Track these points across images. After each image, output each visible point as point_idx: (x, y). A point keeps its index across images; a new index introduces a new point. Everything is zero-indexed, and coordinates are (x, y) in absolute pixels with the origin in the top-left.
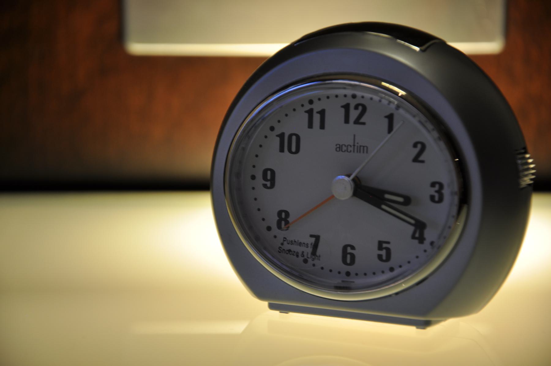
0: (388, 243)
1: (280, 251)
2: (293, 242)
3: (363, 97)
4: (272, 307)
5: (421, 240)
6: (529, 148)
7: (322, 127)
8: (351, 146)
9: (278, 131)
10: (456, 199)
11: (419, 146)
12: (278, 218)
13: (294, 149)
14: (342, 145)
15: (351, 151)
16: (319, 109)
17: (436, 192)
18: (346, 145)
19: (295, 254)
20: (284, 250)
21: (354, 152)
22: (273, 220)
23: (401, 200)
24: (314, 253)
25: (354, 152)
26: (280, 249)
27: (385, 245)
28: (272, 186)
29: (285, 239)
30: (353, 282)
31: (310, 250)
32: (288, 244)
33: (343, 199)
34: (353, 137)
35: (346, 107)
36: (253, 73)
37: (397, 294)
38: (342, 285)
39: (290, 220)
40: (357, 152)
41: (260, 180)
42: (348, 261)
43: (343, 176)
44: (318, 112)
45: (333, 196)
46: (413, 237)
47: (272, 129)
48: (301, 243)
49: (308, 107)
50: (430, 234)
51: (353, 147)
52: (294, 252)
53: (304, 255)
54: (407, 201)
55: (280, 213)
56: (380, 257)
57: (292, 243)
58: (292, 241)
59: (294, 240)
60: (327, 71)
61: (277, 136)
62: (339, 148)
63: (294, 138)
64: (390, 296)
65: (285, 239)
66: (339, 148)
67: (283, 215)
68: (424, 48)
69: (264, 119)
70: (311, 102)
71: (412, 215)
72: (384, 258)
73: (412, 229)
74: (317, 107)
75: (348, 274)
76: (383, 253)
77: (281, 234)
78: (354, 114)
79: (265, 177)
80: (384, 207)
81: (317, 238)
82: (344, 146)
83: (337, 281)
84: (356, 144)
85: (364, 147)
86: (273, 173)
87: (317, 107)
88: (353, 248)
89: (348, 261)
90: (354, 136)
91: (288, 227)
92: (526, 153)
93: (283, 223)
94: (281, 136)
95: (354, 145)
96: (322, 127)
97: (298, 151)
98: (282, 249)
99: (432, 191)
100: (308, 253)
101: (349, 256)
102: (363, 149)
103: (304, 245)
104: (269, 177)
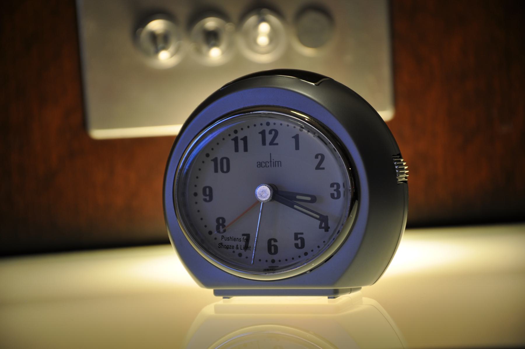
0: (302, 234)
1: (220, 247)
2: (229, 239)
3: (275, 124)
4: (217, 293)
6: (403, 155)
7: (246, 149)
8: (268, 162)
9: (212, 157)
10: (350, 196)
12: (217, 224)
13: (225, 169)
16: (242, 137)
17: (335, 190)
22: (213, 225)
23: (309, 199)
24: (246, 247)
28: (211, 199)
29: (223, 237)
32: (226, 240)
34: (270, 154)
35: (263, 133)
37: (311, 270)
39: (226, 224)
40: (274, 166)
41: (201, 196)
44: (241, 139)
46: (320, 227)
49: (234, 136)
51: (270, 163)
52: (231, 246)
53: (238, 248)
54: (314, 199)
55: (218, 220)
56: (296, 245)
57: (228, 239)
58: (228, 238)
60: (246, 106)
61: (212, 160)
63: (225, 161)
64: (305, 273)
65: (223, 237)
66: (260, 164)
67: (221, 221)
68: (317, 83)
71: (318, 212)
72: (300, 246)
73: (319, 222)
74: (240, 135)
75: (273, 261)
76: (299, 242)
78: (269, 138)
79: (204, 193)
80: (295, 206)
82: (263, 163)
84: (272, 161)
85: (278, 162)
86: (211, 189)
87: (240, 135)
88: (275, 240)
90: (271, 154)
92: (401, 158)
94: (215, 160)
95: (271, 162)
96: (246, 149)
99: (332, 190)
101: (273, 247)
103: (237, 239)
104: (208, 193)
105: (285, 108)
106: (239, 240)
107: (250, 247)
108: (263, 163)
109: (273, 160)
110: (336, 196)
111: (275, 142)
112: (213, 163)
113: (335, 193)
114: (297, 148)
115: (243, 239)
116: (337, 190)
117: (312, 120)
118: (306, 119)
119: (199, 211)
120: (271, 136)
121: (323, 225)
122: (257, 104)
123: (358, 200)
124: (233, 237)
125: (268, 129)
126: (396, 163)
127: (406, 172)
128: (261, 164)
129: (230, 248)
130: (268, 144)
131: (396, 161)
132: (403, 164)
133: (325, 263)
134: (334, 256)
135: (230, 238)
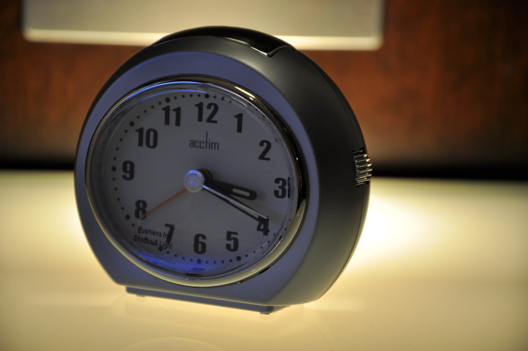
0: (236, 234)
1: (135, 239)
2: (147, 232)
4: (129, 290)
5: (266, 232)
7: (178, 123)
8: (203, 143)
9: (137, 126)
11: (265, 145)
13: (151, 144)
14: (196, 141)
15: (203, 147)
16: (175, 107)
17: (279, 187)
18: (200, 141)
19: (149, 242)
20: (139, 238)
21: (206, 148)
22: (132, 209)
23: (247, 194)
25: (206, 148)
26: (135, 237)
27: (233, 236)
28: (132, 177)
29: (140, 228)
30: (203, 269)
31: (163, 240)
33: (194, 192)
35: (200, 106)
36: (130, 57)
37: (242, 281)
38: (194, 273)
39: (148, 209)
41: (120, 172)
42: (200, 249)
43: (195, 171)
44: (174, 110)
45: (185, 190)
46: (259, 229)
47: (132, 124)
48: (154, 232)
49: (165, 105)
50: (273, 227)
53: (157, 244)
54: (253, 195)
55: (138, 203)
56: (228, 246)
57: (146, 232)
59: (149, 229)
62: (193, 144)
63: (152, 134)
64: (235, 283)
65: (140, 228)
67: (141, 205)
68: (271, 53)
69: (123, 113)
70: (168, 100)
73: (257, 223)
74: (173, 105)
76: (232, 243)
77: (139, 222)
78: (207, 113)
79: (124, 169)
81: (172, 228)
83: (189, 267)
85: (215, 144)
86: (132, 165)
87: (173, 105)
88: (204, 237)
89: (200, 249)
90: (207, 133)
91: (145, 217)
93: (141, 212)
94: (140, 131)
95: (206, 142)
96: (178, 123)
97: (155, 145)
98: (137, 238)
100: (161, 242)
102: (214, 146)
103: (157, 234)
104: (128, 169)
105: (228, 82)
106: (159, 235)
107: (171, 245)
108: (197, 143)
109: (210, 140)
110: (280, 194)
111: (214, 119)
112: (137, 134)
113: (280, 191)
114: (239, 130)
115: (164, 234)
116: (282, 187)
117: (259, 101)
118: (252, 99)
119: (116, 189)
120: (210, 111)
121: (262, 227)
122: (194, 72)
123: (305, 199)
124: (152, 230)
125: (206, 102)
126: (357, 161)
127: (369, 165)
128: (194, 143)
129: (147, 243)
130: (205, 121)
131: (356, 159)
132: (366, 161)
133: (259, 275)
134: (270, 268)
135: (148, 230)
